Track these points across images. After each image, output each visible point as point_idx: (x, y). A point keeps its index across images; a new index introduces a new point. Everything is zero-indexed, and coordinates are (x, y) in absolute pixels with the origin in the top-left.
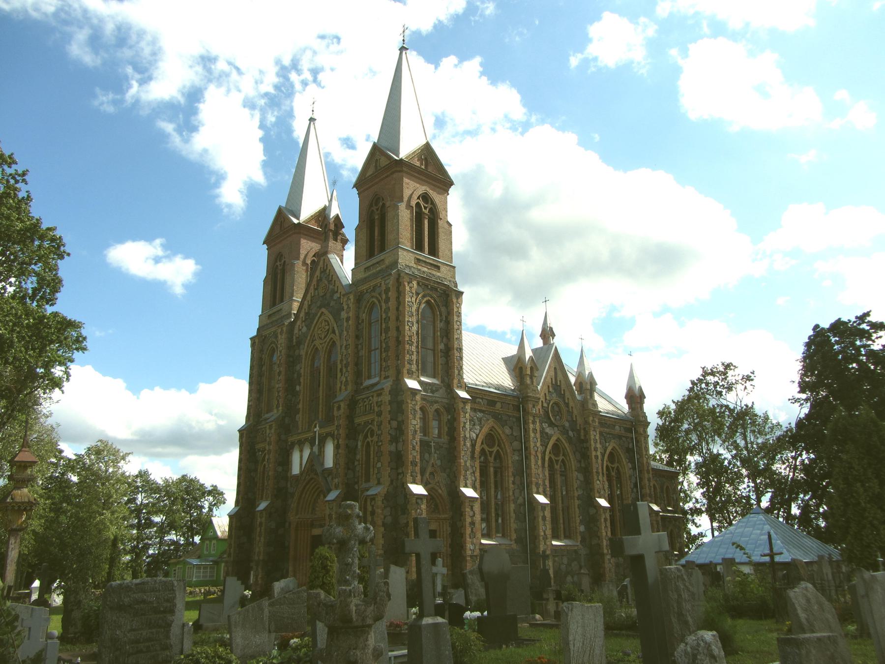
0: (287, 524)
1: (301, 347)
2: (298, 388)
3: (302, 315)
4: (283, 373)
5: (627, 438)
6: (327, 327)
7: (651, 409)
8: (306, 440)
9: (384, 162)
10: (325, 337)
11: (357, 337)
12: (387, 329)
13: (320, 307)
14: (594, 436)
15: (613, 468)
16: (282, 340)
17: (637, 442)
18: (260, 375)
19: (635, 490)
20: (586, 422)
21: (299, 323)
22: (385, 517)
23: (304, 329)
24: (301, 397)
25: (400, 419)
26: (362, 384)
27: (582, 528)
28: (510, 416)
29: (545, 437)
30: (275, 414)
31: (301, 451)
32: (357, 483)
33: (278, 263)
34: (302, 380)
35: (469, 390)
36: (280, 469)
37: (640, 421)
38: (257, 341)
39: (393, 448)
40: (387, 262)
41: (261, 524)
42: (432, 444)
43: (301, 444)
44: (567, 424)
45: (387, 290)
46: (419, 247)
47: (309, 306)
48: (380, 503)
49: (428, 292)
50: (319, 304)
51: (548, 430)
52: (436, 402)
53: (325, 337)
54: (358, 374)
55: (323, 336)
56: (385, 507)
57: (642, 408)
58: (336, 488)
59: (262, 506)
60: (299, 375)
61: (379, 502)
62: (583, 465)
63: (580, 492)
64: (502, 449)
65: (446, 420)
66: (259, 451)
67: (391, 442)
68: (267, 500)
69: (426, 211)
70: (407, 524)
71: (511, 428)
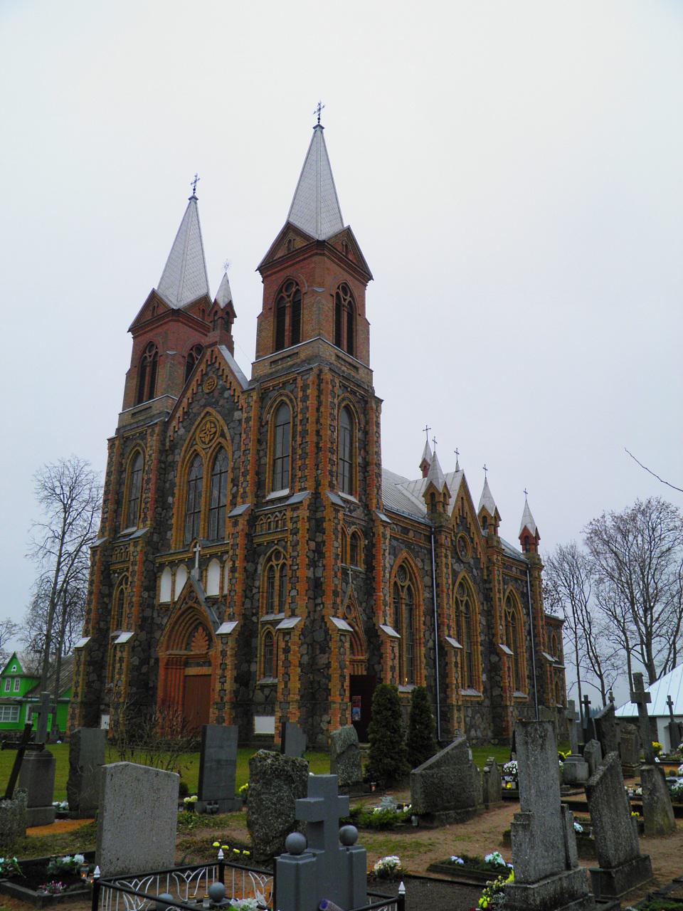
0: (152, 661)
1: (177, 451)
2: (170, 499)
3: (179, 413)
4: (153, 481)
5: (522, 581)
6: (213, 430)
7: (547, 550)
8: (181, 561)
9: (299, 243)
10: (211, 441)
11: (259, 441)
12: (304, 433)
13: (205, 406)
14: (497, 575)
15: (509, 613)
16: (153, 442)
17: (532, 586)
18: (120, 483)
19: (528, 638)
20: (490, 560)
21: (174, 423)
22: (302, 656)
23: (182, 431)
24: (175, 511)
25: (319, 539)
26: (264, 497)
27: (484, 677)
28: (421, 547)
29: (455, 574)
30: (139, 531)
31: (174, 575)
32: (256, 614)
33: (147, 354)
34: (176, 491)
35: (389, 513)
36: (146, 595)
37: (535, 564)
38: (117, 442)
39: (310, 574)
40: (302, 356)
41: (121, 660)
42: (350, 572)
43: (174, 565)
44: (472, 562)
45: (304, 388)
46: (338, 343)
47: (190, 404)
48: (296, 639)
49: (347, 395)
50: (203, 402)
51: (456, 567)
52: (354, 524)
53: (211, 441)
54: (260, 486)
55: (207, 440)
56: (302, 644)
57: (536, 550)
58: (231, 619)
59: (124, 637)
60: (173, 485)
61: (295, 638)
62: (485, 608)
63: (483, 638)
64: (413, 584)
65: (363, 546)
66: (115, 572)
67: (309, 566)
68: (128, 630)
69: (346, 304)
70: (328, 666)
71: (423, 561)
